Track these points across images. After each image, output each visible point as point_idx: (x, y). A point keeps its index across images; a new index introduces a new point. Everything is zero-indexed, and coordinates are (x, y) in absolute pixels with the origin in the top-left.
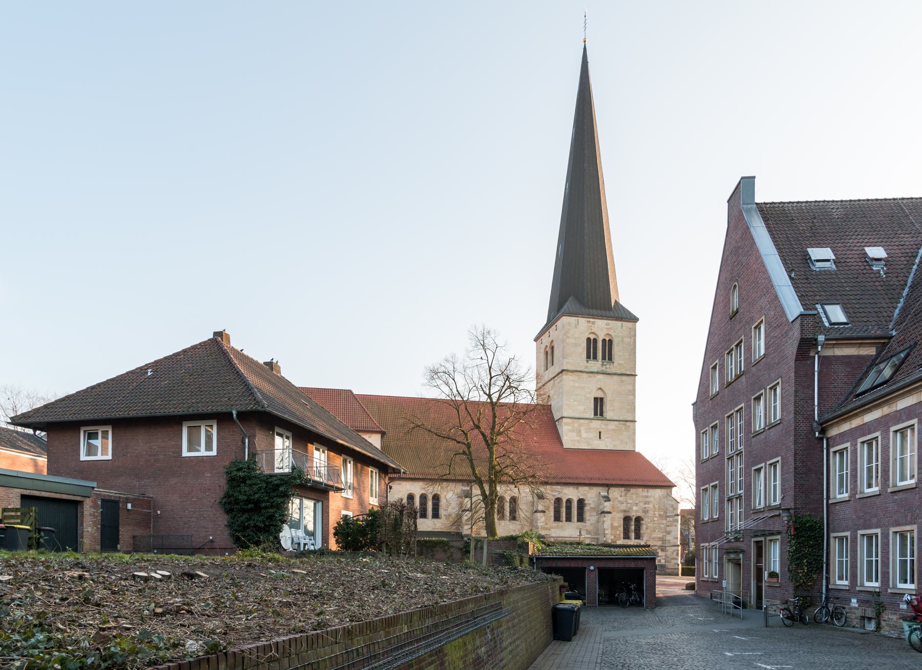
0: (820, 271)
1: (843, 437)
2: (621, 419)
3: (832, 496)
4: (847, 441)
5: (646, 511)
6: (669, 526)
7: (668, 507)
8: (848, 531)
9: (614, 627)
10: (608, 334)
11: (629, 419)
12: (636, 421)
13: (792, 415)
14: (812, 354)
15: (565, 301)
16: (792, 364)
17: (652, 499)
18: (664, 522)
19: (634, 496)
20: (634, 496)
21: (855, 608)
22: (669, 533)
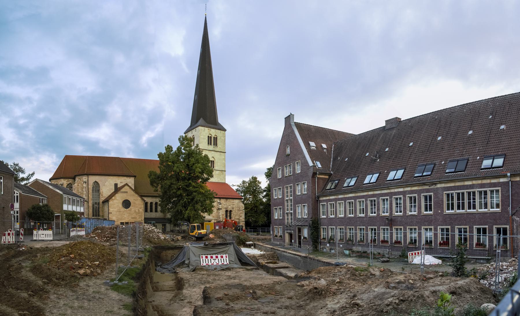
1: (324, 201)
5: (233, 208)
7: (241, 206)
10: (216, 135)
13: (311, 193)
15: (199, 119)
16: (311, 178)
17: (235, 203)
18: (239, 212)
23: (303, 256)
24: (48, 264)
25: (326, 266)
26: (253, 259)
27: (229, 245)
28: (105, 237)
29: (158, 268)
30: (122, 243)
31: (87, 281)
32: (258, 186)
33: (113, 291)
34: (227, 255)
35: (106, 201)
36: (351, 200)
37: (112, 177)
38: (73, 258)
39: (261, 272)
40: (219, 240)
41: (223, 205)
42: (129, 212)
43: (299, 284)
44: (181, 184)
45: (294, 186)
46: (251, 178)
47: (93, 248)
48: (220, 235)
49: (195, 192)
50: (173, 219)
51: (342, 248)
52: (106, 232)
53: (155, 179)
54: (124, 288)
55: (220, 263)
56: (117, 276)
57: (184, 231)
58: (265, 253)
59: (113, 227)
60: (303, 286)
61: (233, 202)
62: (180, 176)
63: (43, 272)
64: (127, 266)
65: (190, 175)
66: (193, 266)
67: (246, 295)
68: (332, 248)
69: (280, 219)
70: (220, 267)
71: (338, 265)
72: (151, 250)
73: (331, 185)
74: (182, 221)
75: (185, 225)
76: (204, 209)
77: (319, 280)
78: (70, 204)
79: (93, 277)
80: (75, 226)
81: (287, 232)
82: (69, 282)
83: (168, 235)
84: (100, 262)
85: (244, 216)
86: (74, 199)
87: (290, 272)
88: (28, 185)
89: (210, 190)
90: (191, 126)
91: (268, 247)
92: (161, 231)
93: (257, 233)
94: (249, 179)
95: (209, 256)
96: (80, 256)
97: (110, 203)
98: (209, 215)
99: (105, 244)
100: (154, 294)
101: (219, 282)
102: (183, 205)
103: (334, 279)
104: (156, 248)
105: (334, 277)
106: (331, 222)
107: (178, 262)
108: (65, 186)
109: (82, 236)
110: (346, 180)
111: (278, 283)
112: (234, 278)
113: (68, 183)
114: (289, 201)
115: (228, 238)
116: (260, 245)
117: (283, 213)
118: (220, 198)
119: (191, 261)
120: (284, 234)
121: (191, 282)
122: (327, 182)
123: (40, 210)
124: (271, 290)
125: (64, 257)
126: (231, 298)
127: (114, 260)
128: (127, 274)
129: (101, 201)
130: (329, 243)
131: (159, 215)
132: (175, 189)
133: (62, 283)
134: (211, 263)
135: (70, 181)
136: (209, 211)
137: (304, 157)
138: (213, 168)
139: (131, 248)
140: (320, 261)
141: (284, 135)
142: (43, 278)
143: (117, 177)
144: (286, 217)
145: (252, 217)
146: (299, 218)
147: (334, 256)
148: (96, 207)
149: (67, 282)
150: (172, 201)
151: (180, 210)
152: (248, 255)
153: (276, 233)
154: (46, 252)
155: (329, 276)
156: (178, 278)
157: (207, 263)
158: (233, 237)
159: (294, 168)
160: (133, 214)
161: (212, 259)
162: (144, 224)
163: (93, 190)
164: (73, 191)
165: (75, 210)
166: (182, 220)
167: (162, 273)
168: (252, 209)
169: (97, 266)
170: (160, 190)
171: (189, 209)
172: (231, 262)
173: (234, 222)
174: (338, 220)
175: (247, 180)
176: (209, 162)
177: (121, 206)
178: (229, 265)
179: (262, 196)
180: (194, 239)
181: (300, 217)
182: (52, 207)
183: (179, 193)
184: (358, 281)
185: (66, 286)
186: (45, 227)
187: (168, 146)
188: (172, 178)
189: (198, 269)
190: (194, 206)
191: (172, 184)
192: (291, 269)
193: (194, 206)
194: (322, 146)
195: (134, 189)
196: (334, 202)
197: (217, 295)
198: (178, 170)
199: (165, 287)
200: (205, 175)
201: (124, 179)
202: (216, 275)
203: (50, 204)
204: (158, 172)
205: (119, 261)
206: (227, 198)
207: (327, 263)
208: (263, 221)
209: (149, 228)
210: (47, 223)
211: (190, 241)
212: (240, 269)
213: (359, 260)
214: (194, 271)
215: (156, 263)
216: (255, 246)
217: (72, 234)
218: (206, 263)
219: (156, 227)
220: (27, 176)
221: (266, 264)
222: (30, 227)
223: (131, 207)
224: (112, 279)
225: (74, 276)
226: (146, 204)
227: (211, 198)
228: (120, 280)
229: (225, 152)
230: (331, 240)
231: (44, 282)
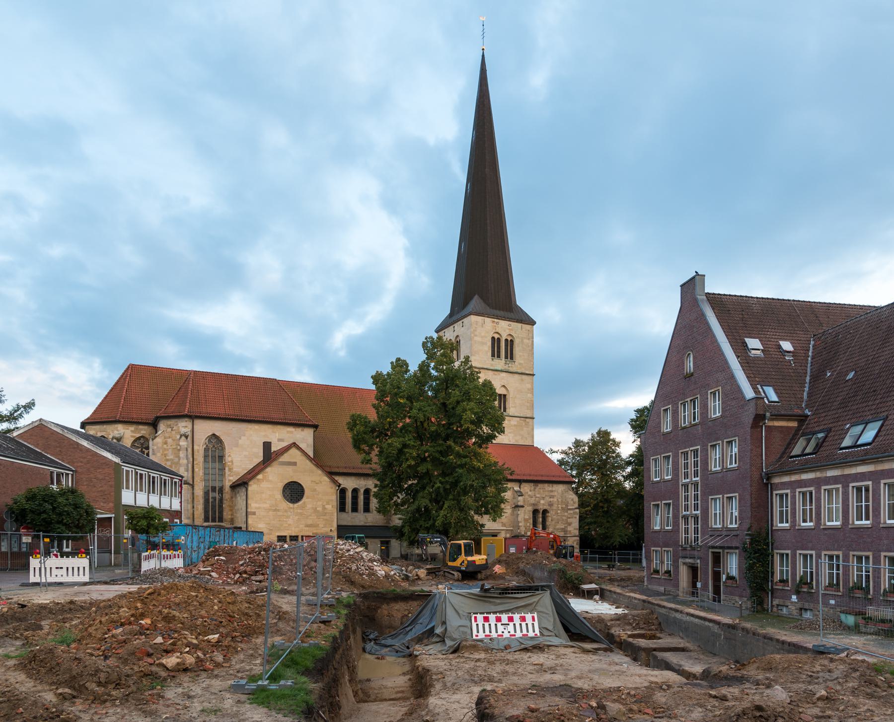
0: (754, 357)
1: (784, 485)
2: (522, 415)
3: (774, 524)
4: (787, 489)
5: (551, 505)
6: (569, 518)
8: (789, 549)
9: (84, 603)
10: (510, 335)
11: (528, 416)
12: (534, 418)
13: (748, 466)
14: (761, 424)
15: (471, 298)
16: (748, 429)
17: (556, 494)
18: (566, 514)
19: (542, 491)
20: (542, 491)
21: (795, 602)
22: (570, 524)
23: (724, 624)
24: (73, 646)
25: (789, 652)
26: (599, 626)
27: (540, 592)
28: (238, 572)
29: (370, 646)
30: (280, 587)
31: (185, 685)
32: (614, 452)
33: (255, 705)
34: (535, 615)
35: (242, 484)
36: (862, 481)
37: (256, 427)
38: (147, 626)
39: (620, 659)
40: (515, 578)
41: (527, 497)
42: (299, 511)
43: (713, 693)
44: (428, 448)
45: (705, 451)
46: (595, 433)
47: (203, 600)
48: (519, 568)
49: (462, 466)
50: (406, 530)
51: (833, 607)
52: (240, 560)
53: (365, 433)
54: (283, 697)
55: (519, 634)
56: (267, 668)
57: (434, 558)
58: (626, 612)
59: (259, 547)
60: (724, 698)
61: (552, 491)
62: (425, 429)
63: (57, 668)
64: (292, 642)
65: (449, 428)
66: (454, 640)
67: (581, 713)
68: (806, 606)
69: (668, 531)
70: (518, 644)
71: (822, 653)
72: (352, 602)
73: (804, 443)
74: (428, 533)
75: (437, 542)
76: (482, 506)
77: (768, 686)
78: (141, 490)
79: (202, 673)
80: (155, 546)
81: (684, 563)
82: (135, 690)
83: (394, 567)
84: (222, 635)
85: (578, 523)
86: (154, 478)
87: (691, 662)
88: (15, 434)
89: (496, 463)
90: (451, 315)
91: (635, 598)
92: (377, 557)
93: (609, 563)
94: (590, 437)
95: (492, 617)
96: (169, 622)
97: (250, 489)
98: (494, 520)
99: (236, 589)
100: (359, 710)
101: (515, 679)
102: (433, 496)
103: (810, 687)
104: (365, 596)
105: (810, 683)
106: (802, 539)
107: (418, 630)
108: (128, 442)
109: (174, 571)
110: (849, 429)
111: (661, 687)
112: (553, 670)
113: (138, 435)
114: (691, 488)
115: (537, 574)
116: (615, 593)
117: (676, 516)
118: (520, 482)
119: (448, 629)
120: (676, 568)
121: (449, 679)
122: (794, 436)
123: (52, 504)
124: (643, 704)
125: (122, 625)
126: (544, 717)
127: (259, 628)
128: (291, 662)
129: (227, 484)
130: (798, 593)
131: (373, 518)
132: (414, 458)
133: (114, 693)
134: (497, 632)
135: (142, 429)
136: (495, 511)
137: (732, 377)
138: (505, 410)
139: (303, 598)
140: (771, 639)
141: (678, 328)
142: (59, 684)
143: (270, 426)
144: (682, 526)
145: (597, 527)
146: (716, 530)
147: (810, 627)
148: (214, 498)
149: (130, 690)
150: (406, 486)
151: (425, 507)
152: (586, 615)
153: (655, 564)
154: (69, 616)
155: (797, 680)
156: (418, 668)
157: (487, 633)
158: (551, 572)
159: (705, 407)
160: (310, 515)
161: (499, 624)
162: (336, 540)
163: (206, 457)
164: (152, 457)
165: (156, 505)
166: (428, 530)
167: (378, 658)
168: (596, 507)
169: (213, 646)
170: (377, 461)
171: (446, 506)
172: (546, 633)
173: (552, 536)
174: (825, 534)
175: (586, 437)
176: (493, 397)
177: (279, 495)
178: (541, 639)
179: (623, 476)
180: (456, 576)
181: (719, 526)
182: (90, 494)
183: (422, 469)
184: (882, 700)
185: (127, 701)
186: (65, 550)
187: (398, 360)
188: (406, 432)
189: (466, 647)
190: (457, 500)
191: (405, 446)
192: (692, 654)
193: (457, 500)
194: (780, 347)
195: (312, 456)
196: (812, 489)
197: (510, 711)
198: (421, 416)
199: (384, 690)
200: (484, 427)
201: (288, 432)
202: (508, 662)
203: (82, 489)
204: (372, 416)
205: (274, 629)
206: (536, 482)
207: (790, 644)
208: (624, 535)
209: (348, 551)
210: (74, 539)
211: (446, 579)
212: (566, 649)
213: (885, 642)
214: (454, 652)
215: (364, 633)
216: (603, 595)
217: (146, 566)
218: (484, 632)
219: (366, 548)
220: (10, 408)
221: (631, 640)
222: (20, 548)
223: (304, 499)
224: (254, 676)
225: (149, 675)
226: (343, 492)
227: (498, 482)
228: (274, 678)
229: (534, 375)
230: (804, 587)
231: (61, 694)
